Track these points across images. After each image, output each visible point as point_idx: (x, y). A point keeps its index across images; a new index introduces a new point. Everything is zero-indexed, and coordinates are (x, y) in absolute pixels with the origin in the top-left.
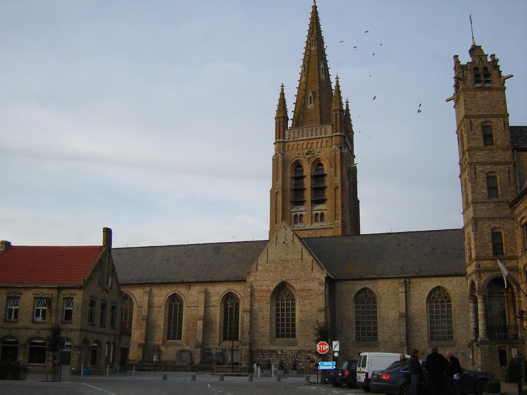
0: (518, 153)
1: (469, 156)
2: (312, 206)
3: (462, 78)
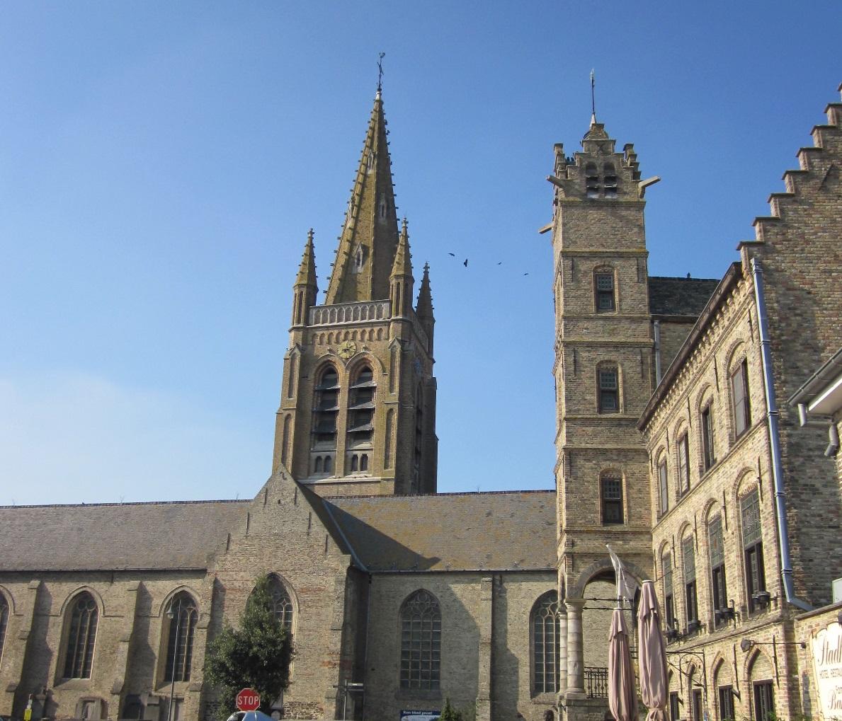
0: (664, 325)
1: (565, 329)
2: (348, 443)
3: (562, 183)
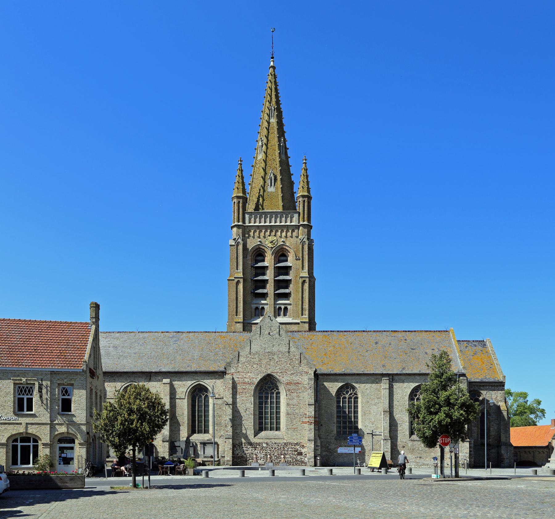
2: (275, 300)
